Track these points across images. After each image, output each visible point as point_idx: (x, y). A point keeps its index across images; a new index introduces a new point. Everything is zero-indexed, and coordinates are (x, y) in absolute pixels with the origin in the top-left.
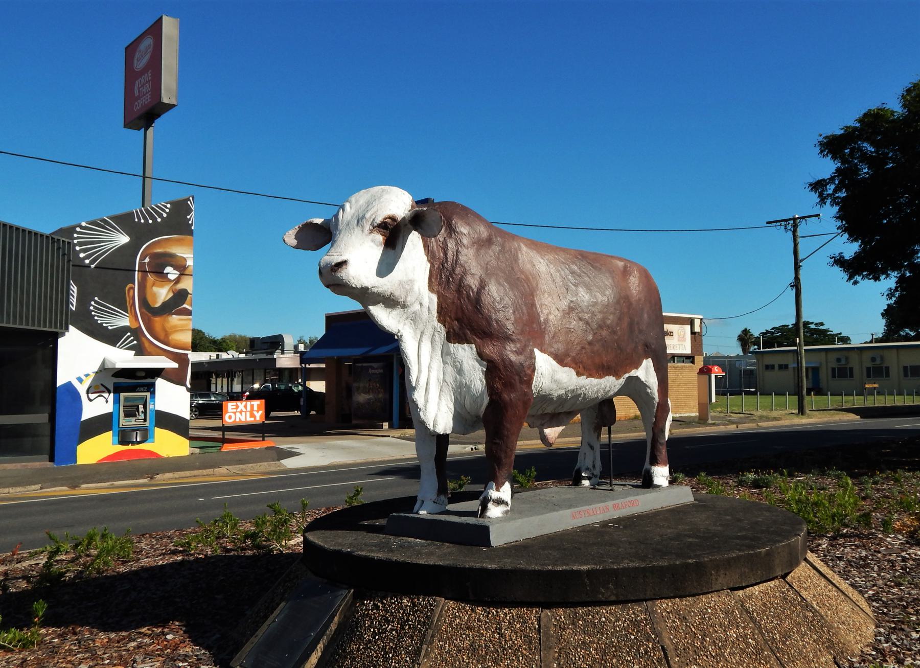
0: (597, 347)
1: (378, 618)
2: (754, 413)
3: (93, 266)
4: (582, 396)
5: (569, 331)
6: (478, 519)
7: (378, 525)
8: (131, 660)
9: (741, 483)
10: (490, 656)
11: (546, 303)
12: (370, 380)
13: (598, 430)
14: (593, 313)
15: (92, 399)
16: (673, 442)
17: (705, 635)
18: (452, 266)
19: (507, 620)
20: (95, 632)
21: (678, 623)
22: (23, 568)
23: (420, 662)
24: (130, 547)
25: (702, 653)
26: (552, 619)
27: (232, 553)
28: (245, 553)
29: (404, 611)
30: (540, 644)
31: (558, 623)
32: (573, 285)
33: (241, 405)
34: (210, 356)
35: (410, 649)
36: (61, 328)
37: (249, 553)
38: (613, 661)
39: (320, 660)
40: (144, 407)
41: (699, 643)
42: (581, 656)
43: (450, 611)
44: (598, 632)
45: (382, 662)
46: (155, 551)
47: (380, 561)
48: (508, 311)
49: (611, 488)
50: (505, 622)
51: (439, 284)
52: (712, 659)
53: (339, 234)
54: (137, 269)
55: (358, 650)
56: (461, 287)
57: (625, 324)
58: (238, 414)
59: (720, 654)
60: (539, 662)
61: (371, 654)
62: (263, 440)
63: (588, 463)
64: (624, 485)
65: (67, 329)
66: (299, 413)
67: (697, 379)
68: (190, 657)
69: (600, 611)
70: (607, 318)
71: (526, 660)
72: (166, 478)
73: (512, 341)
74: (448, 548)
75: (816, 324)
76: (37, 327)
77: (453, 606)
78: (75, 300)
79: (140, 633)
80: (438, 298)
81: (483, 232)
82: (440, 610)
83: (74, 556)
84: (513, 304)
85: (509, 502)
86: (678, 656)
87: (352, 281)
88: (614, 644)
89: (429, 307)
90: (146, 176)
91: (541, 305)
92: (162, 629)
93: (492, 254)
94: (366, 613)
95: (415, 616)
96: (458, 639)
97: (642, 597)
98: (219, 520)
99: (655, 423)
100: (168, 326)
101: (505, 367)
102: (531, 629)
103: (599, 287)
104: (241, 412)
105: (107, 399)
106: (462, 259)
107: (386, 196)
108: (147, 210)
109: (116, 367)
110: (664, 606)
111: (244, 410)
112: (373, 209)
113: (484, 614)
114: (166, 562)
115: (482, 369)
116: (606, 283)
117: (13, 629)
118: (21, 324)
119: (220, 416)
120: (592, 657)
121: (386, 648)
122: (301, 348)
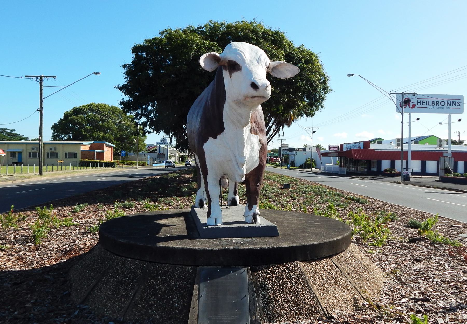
75: (11, 130)
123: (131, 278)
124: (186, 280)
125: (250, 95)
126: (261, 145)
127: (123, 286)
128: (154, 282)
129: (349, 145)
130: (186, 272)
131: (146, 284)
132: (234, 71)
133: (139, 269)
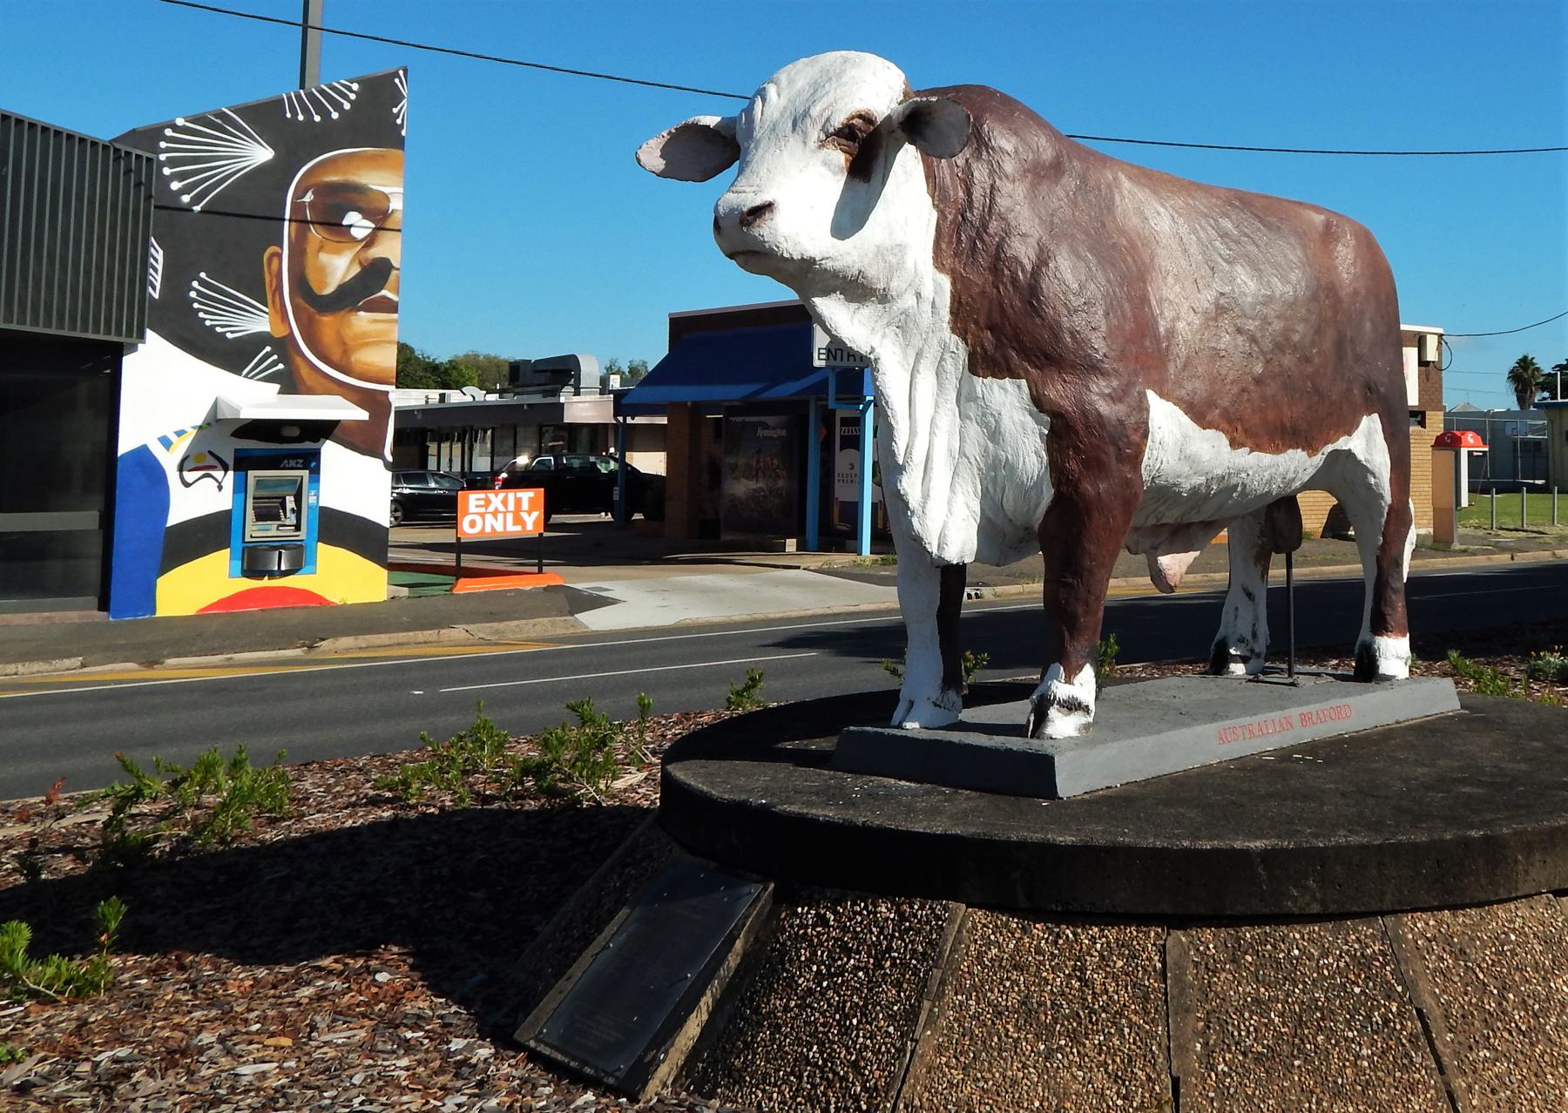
0: (1272, 389)
1: (826, 944)
2: (1546, 529)
3: (197, 208)
4: (1239, 489)
5: (1216, 355)
6: (1029, 740)
7: (815, 751)
8: (307, 1025)
9: (1534, 674)
10: (1062, 1025)
11: (1171, 298)
12: (759, 452)
13: (1263, 561)
14: (1265, 321)
15: (190, 482)
16: (1416, 583)
17: (1504, 988)
18: (982, 217)
19: (1096, 950)
20: (223, 966)
21: (1450, 961)
22: (63, 830)
23: (917, 1036)
24: (282, 789)
25: (1499, 1024)
26: (1189, 950)
27: (496, 805)
28: (522, 805)
29: (882, 929)
30: (1166, 1001)
31: (1202, 959)
32: (1225, 260)
33: (496, 498)
34: (427, 397)
35: (896, 1008)
36: (129, 333)
37: (531, 805)
38: (1319, 1039)
39: (706, 1030)
40: (295, 501)
41: (1493, 1005)
42: (1252, 1029)
43: (977, 930)
44: (1286, 979)
45: (837, 1035)
46: (335, 798)
47: (830, 826)
48: (1096, 313)
49: (1290, 680)
50: (1092, 956)
51: (956, 255)
52: (1521, 1037)
53: (756, 148)
54: (287, 216)
55: (786, 1009)
56: (999, 262)
57: (1328, 344)
58: (489, 518)
59: (1537, 1026)
60: (1166, 1040)
61: (813, 1018)
62: (540, 571)
63: (1244, 628)
64: (1318, 675)
65: (142, 337)
66: (609, 517)
67: (1430, 457)
68: (429, 1020)
69: (1288, 935)
70: (1292, 330)
71: (1138, 1034)
72: (339, 648)
73: (1102, 374)
74: (967, 799)
76: (93, 333)
77: (984, 921)
78: (159, 278)
79: (320, 969)
80: (954, 283)
81: (1046, 149)
82: (956, 929)
83: (167, 806)
84: (1104, 297)
85: (1092, 707)
86: (1451, 1031)
87: (783, 246)
88: (1320, 1004)
89: (934, 302)
90: (310, 24)
91: (1161, 301)
92: (366, 961)
93: (1062, 194)
94: (801, 932)
95: (904, 941)
96: (996, 990)
97: (1375, 907)
98: (465, 736)
99: (1382, 548)
100: (348, 334)
101: (1087, 428)
102: (1146, 970)
103: (1276, 266)
104: (495, 513)
105: (220, 483)
106: (1002, 202)
107: (852, 73)
108: (310, 96)
109: (242, 417)
110: (1419, 925)
111: (501, 508)
112: (825, 99)
113: (1047, 939)
114: (361, 820)
115: (1040, 430)
116: (1291, 257)
117: (55, 958)
118: (85, 330)
119: (453, 522)
120: (1275, 1030)
121: (844, 1007)
122: (615, 382)
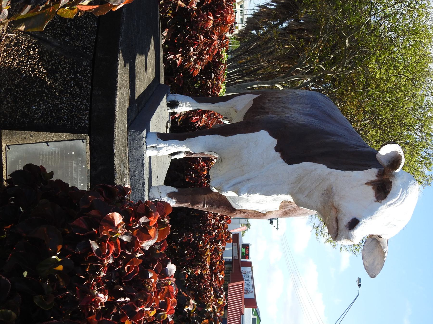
123: (70, 31)
124: (70, 117)
125: (340, 216)
126: (264, 213)
127: (58, 20)
128: (65, 69)
129: (250, 276)
130: (80, 116)
131: (62, 57)
132: (375, 190)
133: (84, 43)
